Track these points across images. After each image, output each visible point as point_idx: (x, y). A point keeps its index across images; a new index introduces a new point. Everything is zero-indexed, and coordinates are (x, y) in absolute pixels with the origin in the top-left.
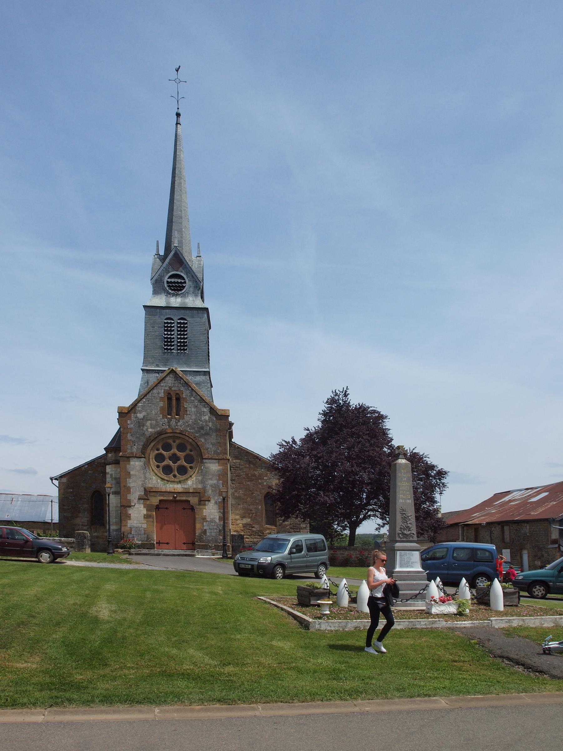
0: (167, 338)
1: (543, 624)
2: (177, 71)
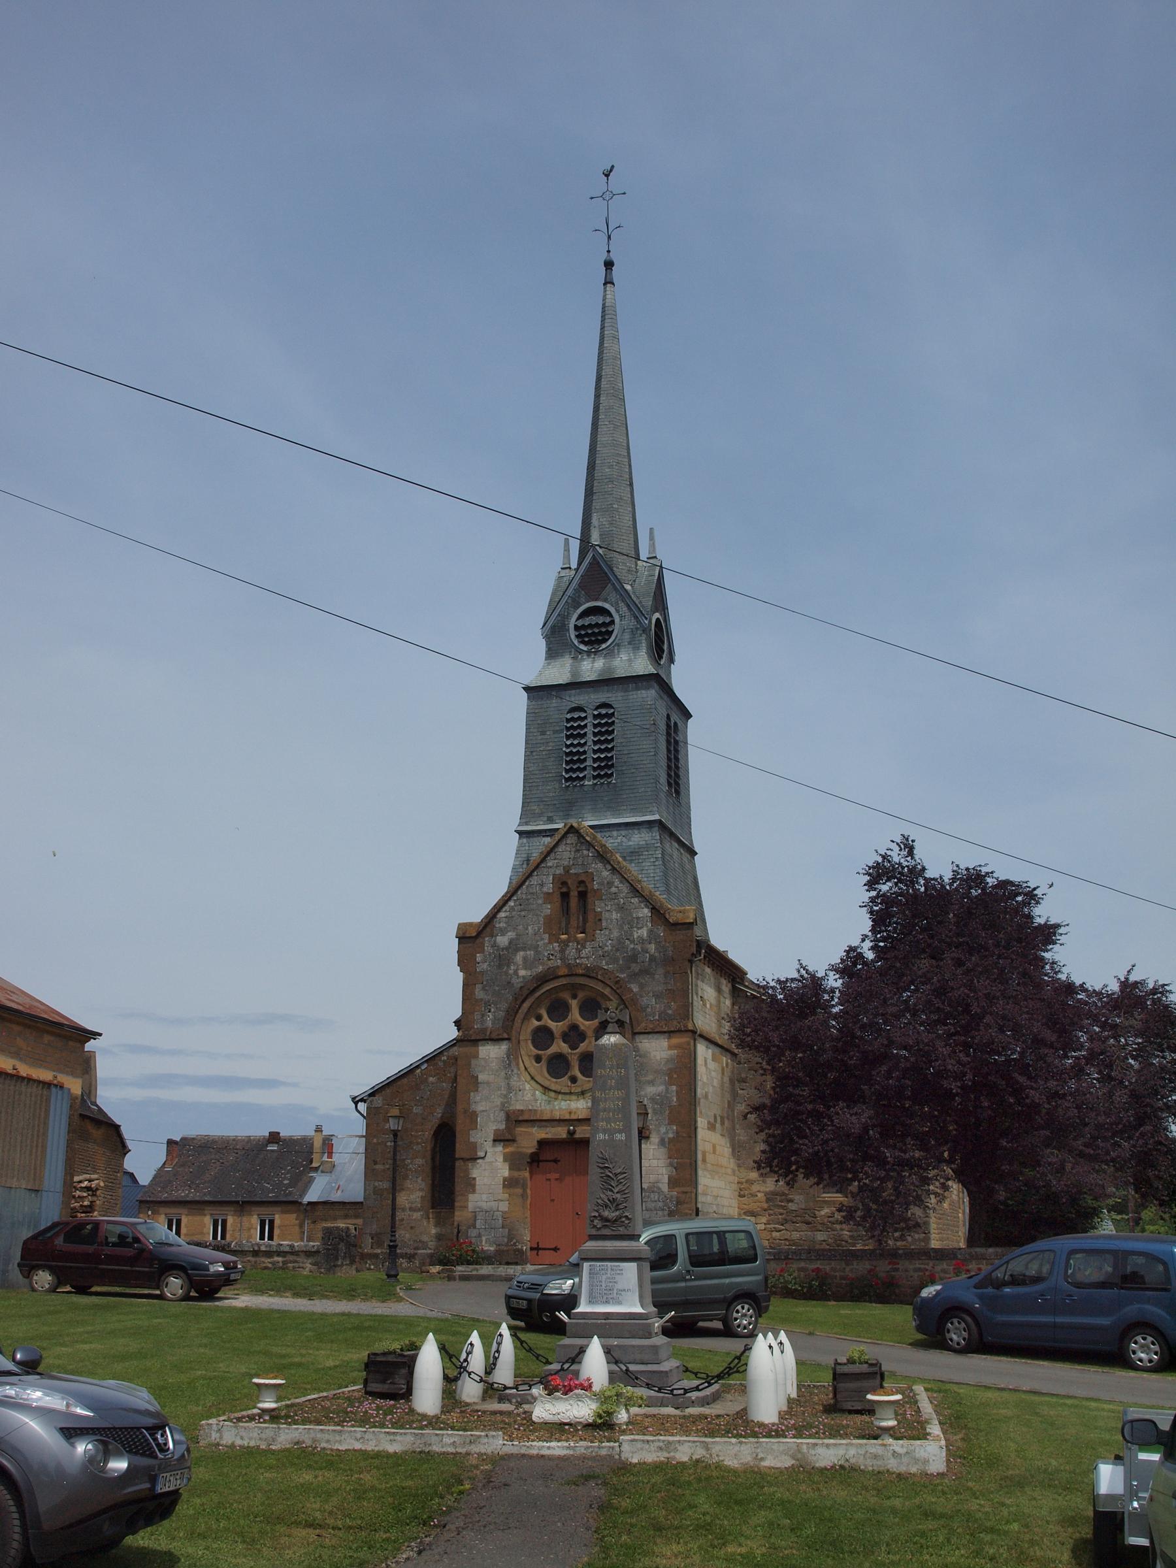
0: (571, 753)
1: (762, 1459)
2: (607, 176)
